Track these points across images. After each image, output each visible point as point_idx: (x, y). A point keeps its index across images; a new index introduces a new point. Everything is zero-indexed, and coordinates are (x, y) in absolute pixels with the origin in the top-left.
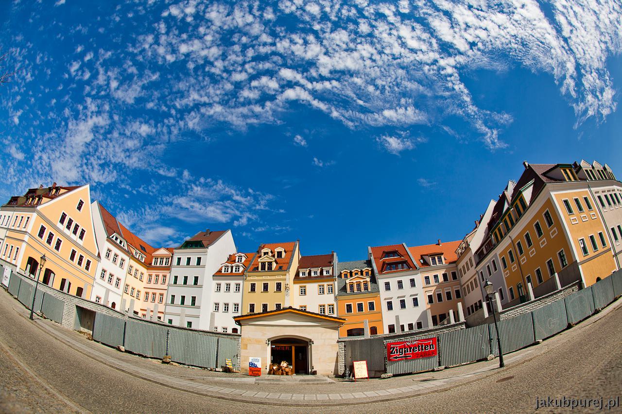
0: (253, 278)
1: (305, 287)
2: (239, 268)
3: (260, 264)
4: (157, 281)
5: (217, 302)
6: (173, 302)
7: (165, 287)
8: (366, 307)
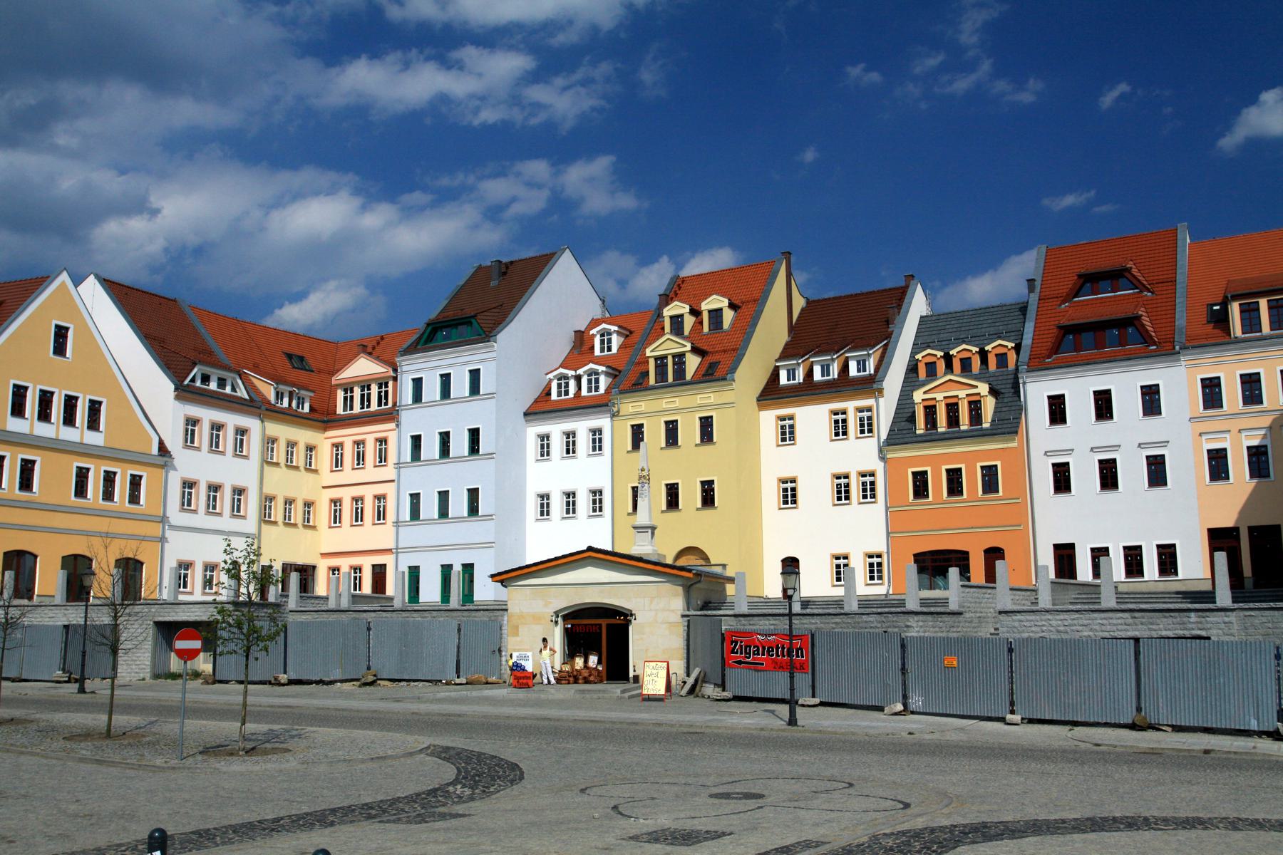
1: (791, 418)
2: (597, 381)
3: (652, 363)
4: (360, 458)
6: (415, 514)
7: (388, 472)
8: (973, 482)
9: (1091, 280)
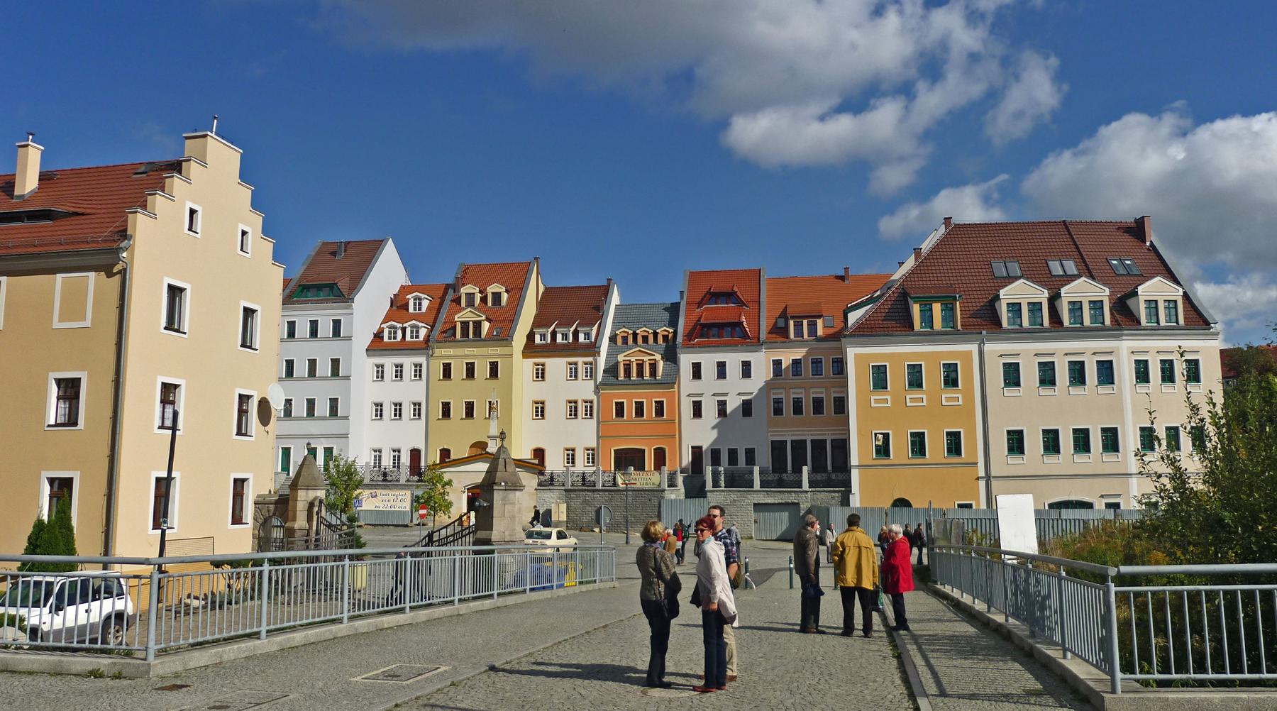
0: (444, 353)
3: (459, 325)
5: (378, 401)
9: (715, 296)
